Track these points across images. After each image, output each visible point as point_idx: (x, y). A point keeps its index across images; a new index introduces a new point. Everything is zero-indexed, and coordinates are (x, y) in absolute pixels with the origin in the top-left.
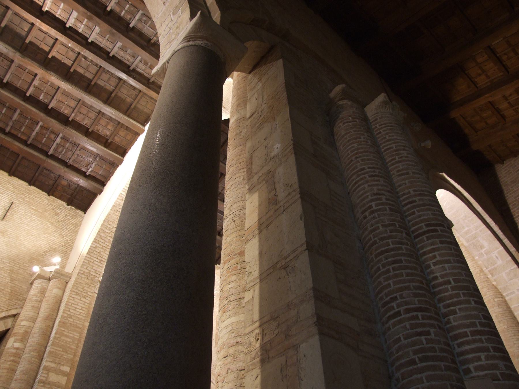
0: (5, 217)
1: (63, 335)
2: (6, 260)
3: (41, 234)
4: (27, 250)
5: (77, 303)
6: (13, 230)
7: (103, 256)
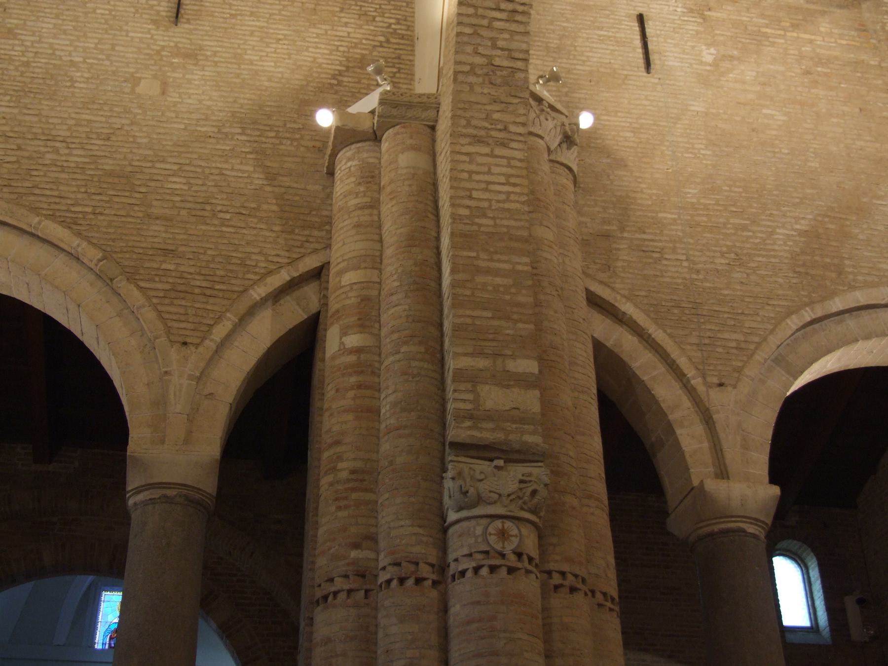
0: (182, 11)
1: (479, 270)
2: (231, 127)
6: (218, 41)
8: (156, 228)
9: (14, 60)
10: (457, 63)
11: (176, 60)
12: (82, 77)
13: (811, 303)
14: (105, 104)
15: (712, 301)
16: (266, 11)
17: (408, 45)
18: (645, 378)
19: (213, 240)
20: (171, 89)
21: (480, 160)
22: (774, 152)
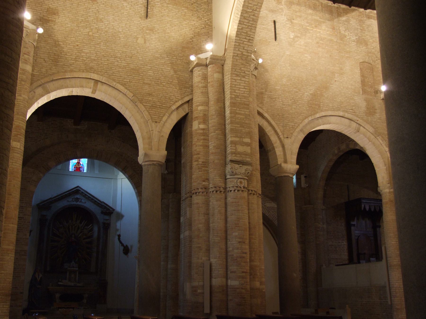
1: (237, 113)
3: (182, 22)
4: (177, 41)
5: (239, 84)
7: (250, 35)
8: (146, 87)
9: (103, 30)
10: (234, 53)
11: (147, 32)
12: (122, 36)
13: (311, 115)
14: (129, 46)
15: (287, 114)
16: (171, 15)
17: (211, 28)
18: (269, 134)
19: (161, 91)
20: (147, 42)
21: (238, 81)
22: (306, 69)
